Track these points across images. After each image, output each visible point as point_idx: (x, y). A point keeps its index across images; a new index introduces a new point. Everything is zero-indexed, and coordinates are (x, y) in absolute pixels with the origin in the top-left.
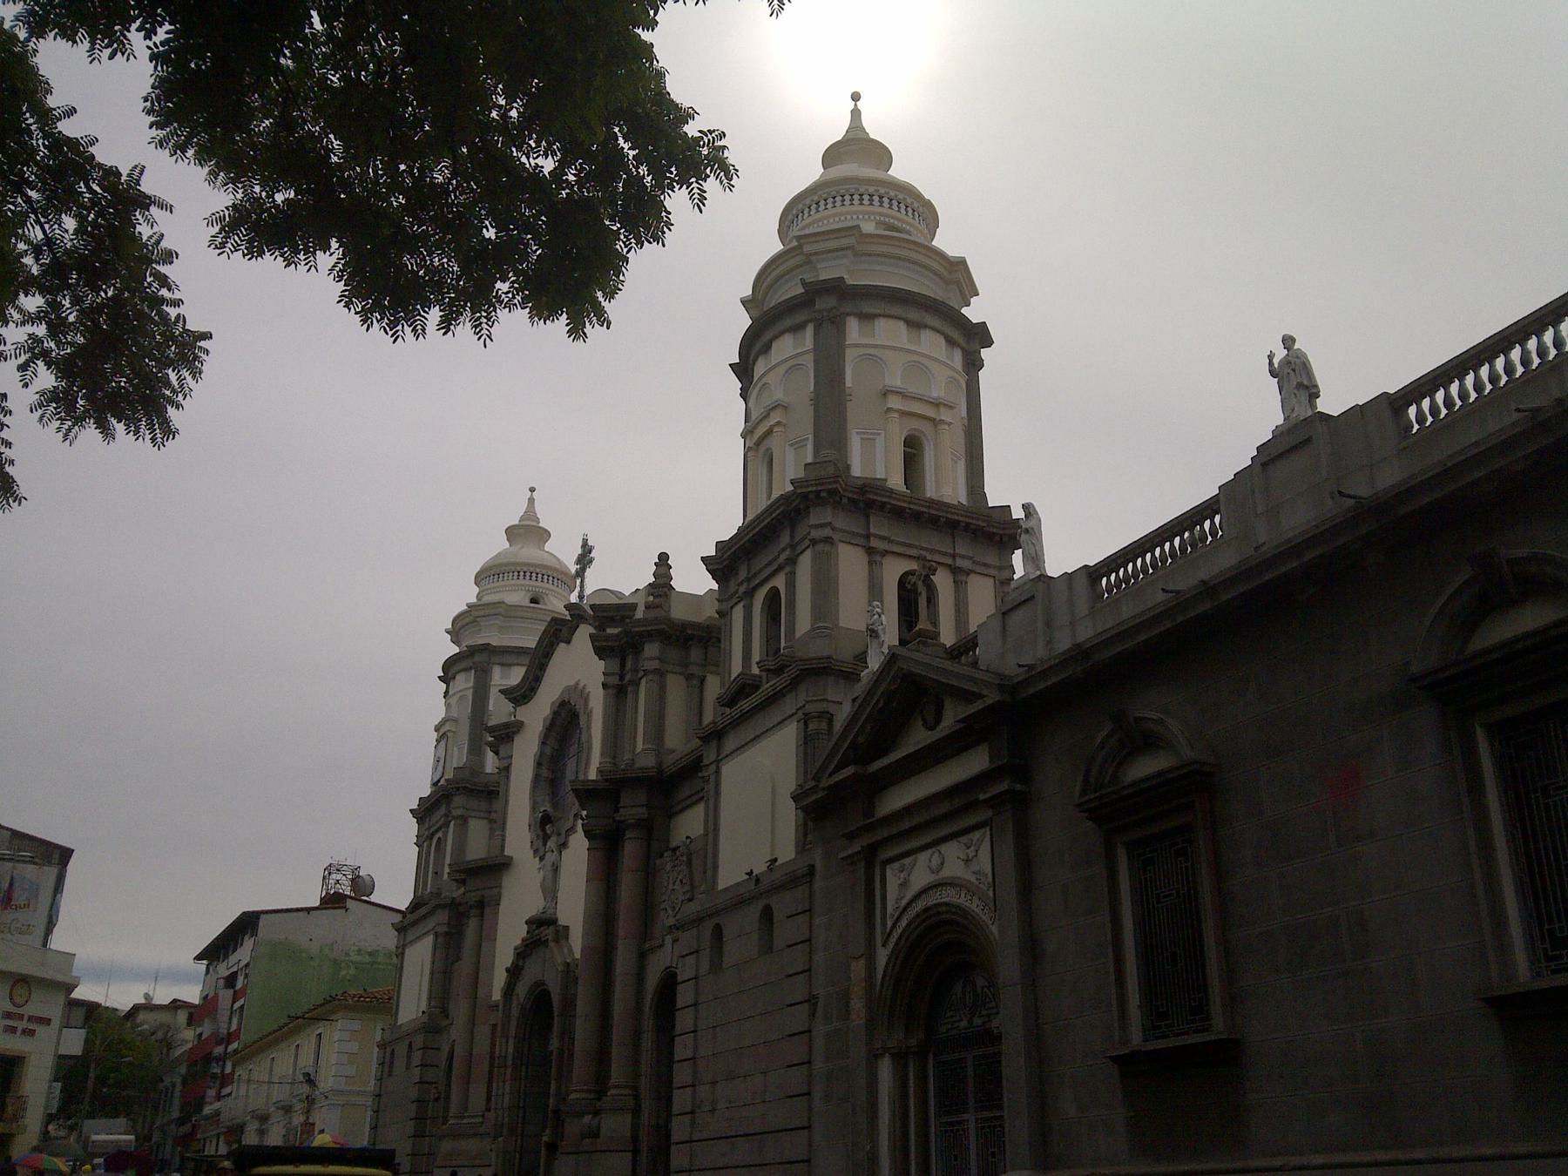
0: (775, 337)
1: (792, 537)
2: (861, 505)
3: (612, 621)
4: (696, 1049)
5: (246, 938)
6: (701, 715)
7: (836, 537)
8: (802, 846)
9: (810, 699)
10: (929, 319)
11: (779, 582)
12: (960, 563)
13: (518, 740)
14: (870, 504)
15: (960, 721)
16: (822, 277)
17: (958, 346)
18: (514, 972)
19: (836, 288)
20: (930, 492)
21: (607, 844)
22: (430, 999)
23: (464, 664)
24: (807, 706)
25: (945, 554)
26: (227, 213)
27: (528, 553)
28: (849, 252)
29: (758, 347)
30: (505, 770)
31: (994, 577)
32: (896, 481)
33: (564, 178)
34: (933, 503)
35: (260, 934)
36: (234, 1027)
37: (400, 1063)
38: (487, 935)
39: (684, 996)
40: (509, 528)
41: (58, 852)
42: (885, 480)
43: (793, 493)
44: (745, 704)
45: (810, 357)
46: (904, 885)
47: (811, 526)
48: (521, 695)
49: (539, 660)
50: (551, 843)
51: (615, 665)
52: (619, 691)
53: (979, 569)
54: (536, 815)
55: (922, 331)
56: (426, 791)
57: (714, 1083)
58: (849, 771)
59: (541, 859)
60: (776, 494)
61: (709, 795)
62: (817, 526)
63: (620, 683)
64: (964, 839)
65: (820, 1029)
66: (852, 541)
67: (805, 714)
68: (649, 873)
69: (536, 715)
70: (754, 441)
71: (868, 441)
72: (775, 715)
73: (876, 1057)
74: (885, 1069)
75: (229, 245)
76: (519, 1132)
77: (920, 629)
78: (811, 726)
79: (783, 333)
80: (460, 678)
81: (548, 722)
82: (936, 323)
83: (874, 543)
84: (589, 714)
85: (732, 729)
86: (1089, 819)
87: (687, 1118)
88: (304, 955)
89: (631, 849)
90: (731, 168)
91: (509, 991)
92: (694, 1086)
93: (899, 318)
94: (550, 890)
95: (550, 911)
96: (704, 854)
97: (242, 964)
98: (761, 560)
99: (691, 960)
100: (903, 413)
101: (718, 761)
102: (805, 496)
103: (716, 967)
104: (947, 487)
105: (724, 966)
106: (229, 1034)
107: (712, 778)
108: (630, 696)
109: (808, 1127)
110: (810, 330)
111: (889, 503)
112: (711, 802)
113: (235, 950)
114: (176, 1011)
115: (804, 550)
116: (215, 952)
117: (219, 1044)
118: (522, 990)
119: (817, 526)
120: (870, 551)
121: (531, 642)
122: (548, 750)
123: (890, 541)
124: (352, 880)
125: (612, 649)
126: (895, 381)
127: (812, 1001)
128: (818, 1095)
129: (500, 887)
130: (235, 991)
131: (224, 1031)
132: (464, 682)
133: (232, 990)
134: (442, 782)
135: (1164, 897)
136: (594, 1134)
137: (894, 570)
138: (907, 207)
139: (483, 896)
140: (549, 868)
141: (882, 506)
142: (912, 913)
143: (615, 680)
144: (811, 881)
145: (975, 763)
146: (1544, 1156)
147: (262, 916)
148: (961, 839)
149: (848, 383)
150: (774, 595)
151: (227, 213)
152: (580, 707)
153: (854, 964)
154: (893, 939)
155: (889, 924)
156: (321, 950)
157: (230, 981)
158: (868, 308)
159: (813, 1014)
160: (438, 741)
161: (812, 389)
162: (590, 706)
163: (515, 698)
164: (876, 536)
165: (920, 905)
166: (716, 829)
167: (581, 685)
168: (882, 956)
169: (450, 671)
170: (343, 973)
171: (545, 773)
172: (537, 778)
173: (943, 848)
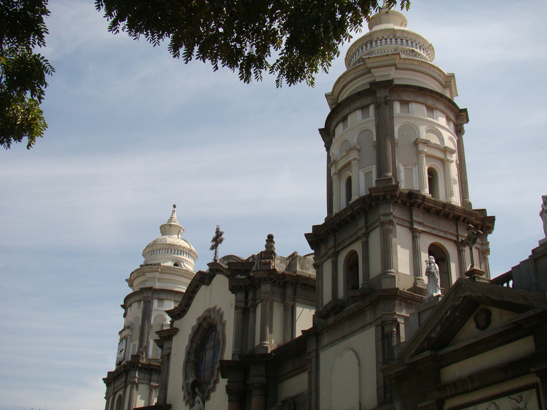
0: (350, 113)
1: (366, 222)
3: (239, 272)
6: (449, 286)
7: (395, 221)
10: (344, 113)
11: (357, 247)
13: (175, 339)
15: (514, 323)
19: (388, 84)
23: (137, 298)
24: (384, 317)
25: (451, 234)
28: (393, 68)
30: (167, 357)
31: (479, 249)
33: (196, 44)
40: (162, 226)
42: (419, 191)
50: (198, 398)
51: (241, 296)
54: (187, 381)
58: (426, 354)
60: (355, 197)
62: (384, 215)
63: (245, 306)
64: (515, 396)
66: (403, 224)
67: (383, 322)
70: (337, 170)
75: (275, 68)
79: (356, 110)
80: (135, 306)
81: (195, 329)
84: (224, 324)
101: (317, 350)
102: (378, 198)
107: (314, 360)
108: (251, 315)
110: (372, 109)
114: (389, 103)
119: (384, 215)
120: (413, 231)
122: (194, 345)
132: (136, 310)
134: (123, 363)
137: (425, 242)
138: (412, 43)
143: (242, 304)
148: (511, 396)
149: (396, 136)
150: (354, 254)
160: (121, 340)
162: (224, 320)
164: (416, 222)
166: (317, 390)
171: (192, 358)
172: (187, 362)
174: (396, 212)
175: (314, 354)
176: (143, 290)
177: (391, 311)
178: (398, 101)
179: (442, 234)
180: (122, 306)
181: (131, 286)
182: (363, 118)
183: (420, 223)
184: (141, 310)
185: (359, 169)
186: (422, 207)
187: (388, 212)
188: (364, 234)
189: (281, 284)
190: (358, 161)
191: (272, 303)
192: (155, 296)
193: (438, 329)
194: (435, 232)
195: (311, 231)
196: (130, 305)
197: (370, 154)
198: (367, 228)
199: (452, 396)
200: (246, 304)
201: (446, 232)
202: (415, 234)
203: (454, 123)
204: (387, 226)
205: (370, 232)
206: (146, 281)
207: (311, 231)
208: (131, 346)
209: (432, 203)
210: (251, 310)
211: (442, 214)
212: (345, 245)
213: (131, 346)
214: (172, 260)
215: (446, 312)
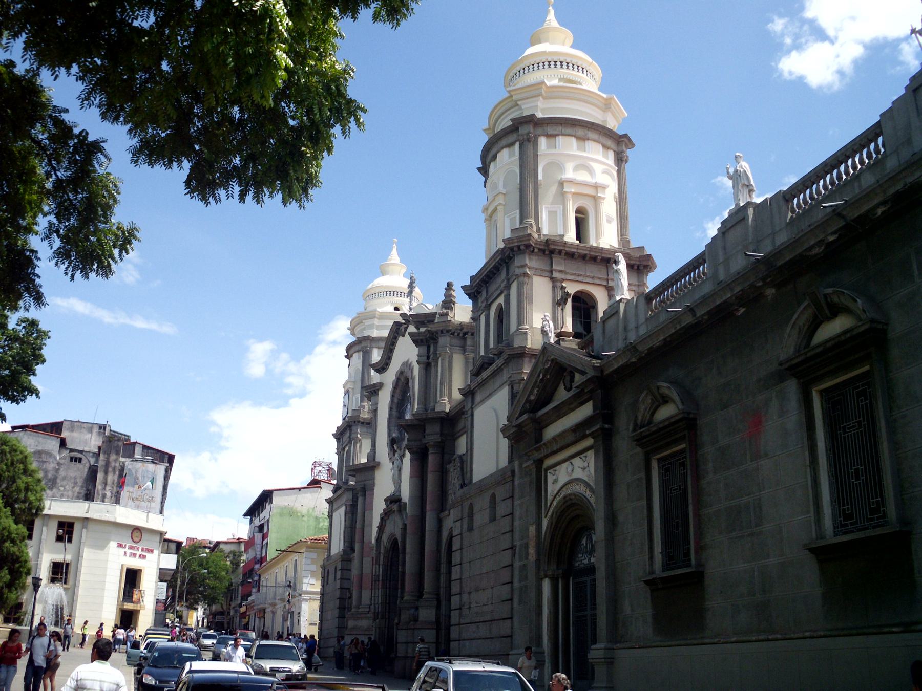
0: (498, 152)
2: (547, 252)
4: (461, 573)
5: (268, 504)
8: (511, 460)
9: (514, 372)
10: (592, 135)
11: (501, 300)
13: (380, 393)
14: (552, 252)
16: (525, 114)
17: (611, 149)
18: (381, 528)
20: (593, 242)
21: (420, 457)
22: (344, 542)
23: (357, 348)
25: (600, 279)
26: (138, 144)
29: (490, 155)
30: (375, 411)
32: (571, 237)
34: (592, 248)
35: (274, 502)
36: (264, 555)
37: (331, 577)
38: (368, 507)
39: (456, 545)
41: (167, 456)
43: (505, 248)
44: (485, 374)
46: (555, 481)
47: (515, 267)
48: (382, 368)
49: (390, 345)
52: (427, 365)
55: (587, 142)
56: (339, 423)
57: (470, 593)
58: (525, 416)
59: (393, 463)
61: (469, 431)
62: (519, 267)
65: (517, 564)
67: (511, 381)
68: (443, 473)
69: (389, 378)
72: (499, 381)
73: (542, 579)
74: (546, 585)
75: (140, 161)
76: (387, 617)
78: (516, 388)
79: (502, 148)
80: (355, 356)
83: (555, 275)
84: (413, 379)
85: (479, 389)
86: (639, 445)
87: (457, 611)
88: (299, 514)
89: (432, 460)
90: (348, 128)
91: (379, 539)
92: (460, 594)
94: (398, 482)
95: (397, 494)
96: (465, 463)
97: (266, 519)
98: (492, 288)
99: (458, 524)
101: (472, 408)
102: (512, 249)
103: (470, 529)
105: (474, 528)
106: (261, 558)
109: (511, 618)
111: (564, 250)
112: (469, 432)
113: (262, 511)
115: (514, 281)
116: (254, 510)
117: (256, 563)
118: (385, 538)
119: (519, 267)
120: (553, 280)
121: (385, 333)
122: (396, 400)
124: (328, 470)
125: (422, 340)
127: (513, 548)
128: (516, 600)
129: (374, 478)
130: (263, 535)
131: (258, 557)
132: (357, 358)
133: (262, 534)
135: (674, 490)
136: (416, 619)
139: (365, 485)
140: (396, 469)
141: (560, 252)
142: (558, 498)
144: (513, 480)
145: (586, 411)
146: (830, 636)
147: (274, 492)
149: (540, 177)
151: (138, 144)
152: (409, 374)
153: (531, 528)
154: (550, 514)
155: (548, 504)
156: (308, 511)
157: (261, 528)
158: (551, 130)
159: (514, 555)
161: (519, 182)
163: (378, 369)
164: (556, 271)
165: (563, 494)
166: (472, 449)
167: (410, 362)
168: (545, 523)
170: (321, 524)
173: (573, 461)
174: (531, 262)
175: (470, 412)
177: (519, 370)
178: (544, 135)
182: (510, 157)
183: (561, 271)
185: (505, 214)
186: (563, 254)
187: (523, 264)
188: (505, 287)
189: (461, 335)
190: (504, 205)
191: (451, 357)
192: (374, 345)
193: (536, 391)
194: (581, 279)
195: (468, 283)
196: (352, 356)
198: (508, 280)
199: (548, 456)
201: (593, 278)
203: (614, 151)
204: (522, 279)
205: (511, 284)
206: (364, 329)
207: (468, 283)
208: (354, 398)
209: (575, 248)
210: (433, 364)
211: (587, 258)
212: (494, 298)
213: (354, 398)
214: (392, 304)
215: (539, 376)
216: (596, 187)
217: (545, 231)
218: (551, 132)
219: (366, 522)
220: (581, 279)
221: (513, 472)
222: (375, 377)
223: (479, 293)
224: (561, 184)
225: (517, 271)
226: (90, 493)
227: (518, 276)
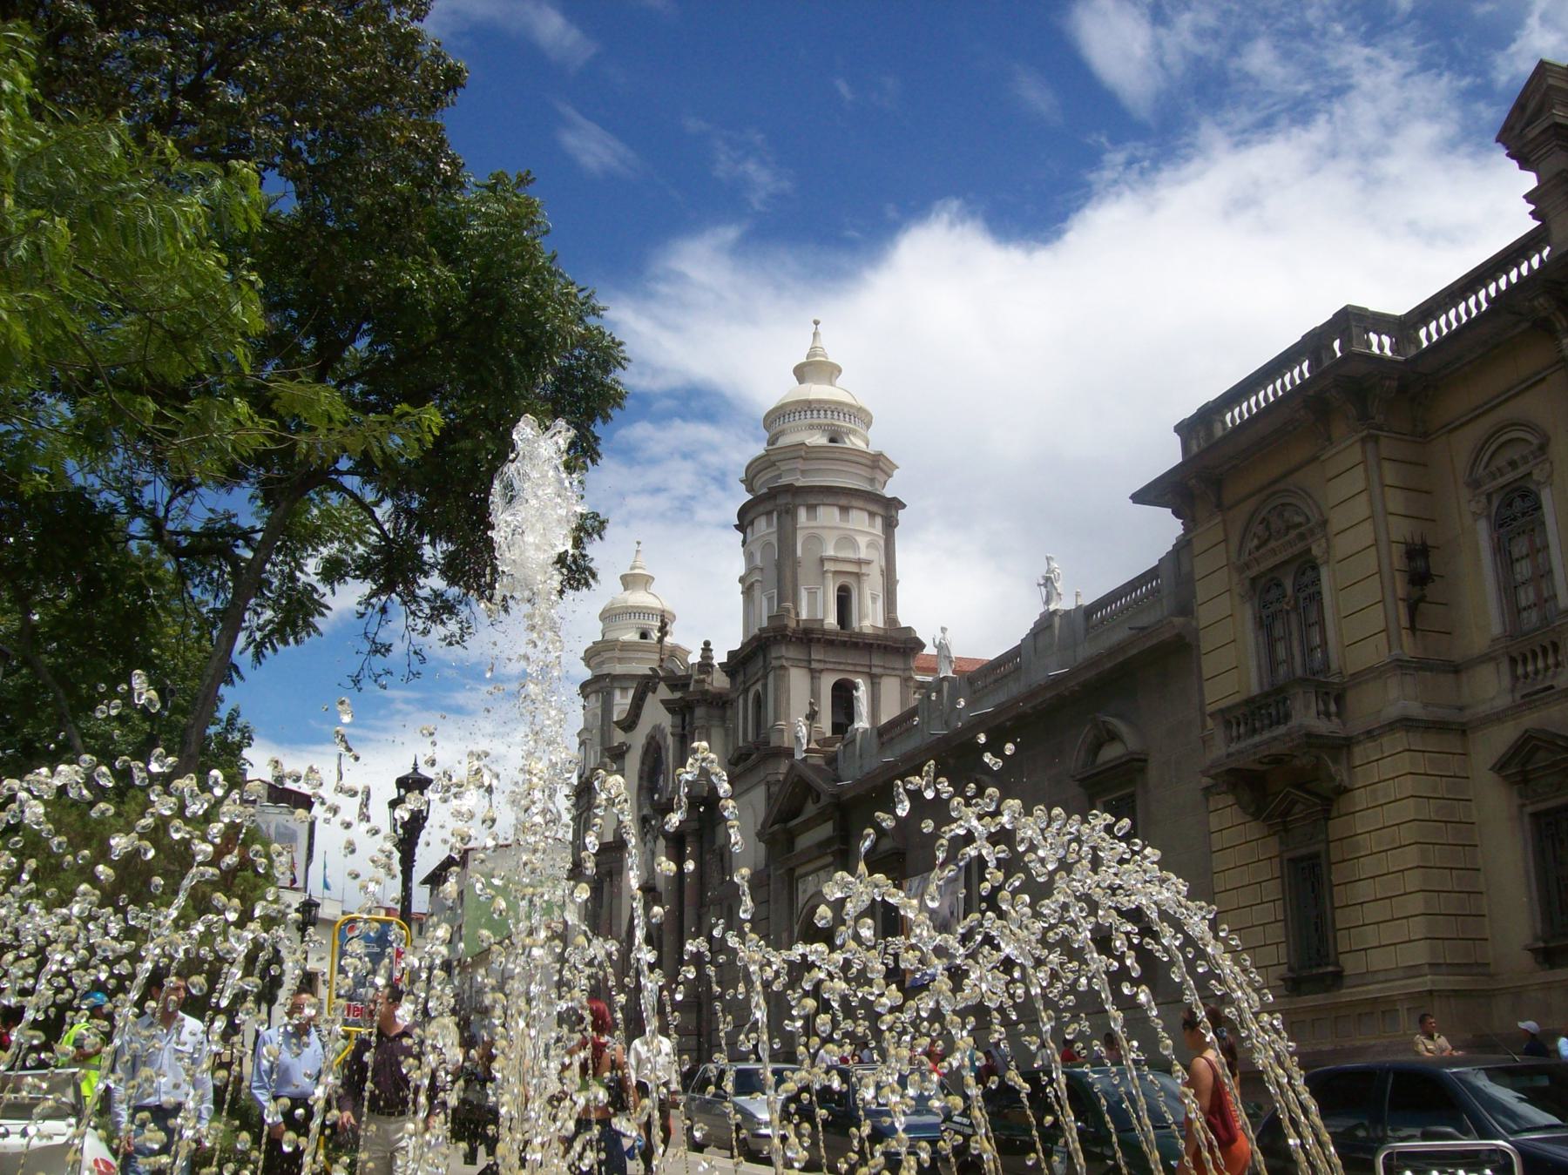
10: (855, 503)
11: (759, 687)
12: (874, 670)
27: (817, 391)
32: (831, 621)
45: (775, 535)
46: (805, 891)
51: (678, 721)
53: (889, 672)
58: (776, 827)
69: (638, 739)
71: (812, 594)
77: (640, 888)
78: (772, 789)
82: (860, 504)
83: (814, 665)
93: (833, 505)
100: (836, 573)
102: (768, 638)
104: (870, 619)
110: (775, 515)
114: (791, 512)
122: (646, 769)
123: (825, 662)
126: (830, 552)
137: (827, 682)
141: (819, 640)
143: (679, 730)
149: (799, 552)
169: (586, 689)
171: (645, 784)
174: (791, 652)
176: (774, 493)
179: (850, 668)
180: (737, 527)
181: (750, 490)
183: (819, 661)
184: (599, 704)
194: (842, 667)
196: (752, 523)
197: (772, 574)
199: (802, 864)
200: (684, 728)
202: (814, 674)
206: (603, 663)
216: (859, 562)
217: (804, 615)
218: (812, 501)
219: (614, 912)
220: (842, 667)
221: (769, 876)
222: (619, 737)
223: (737, 672)
224: (822, 560)
225: (775, 663)
226: (603, 1017)
227: (774, 668)
